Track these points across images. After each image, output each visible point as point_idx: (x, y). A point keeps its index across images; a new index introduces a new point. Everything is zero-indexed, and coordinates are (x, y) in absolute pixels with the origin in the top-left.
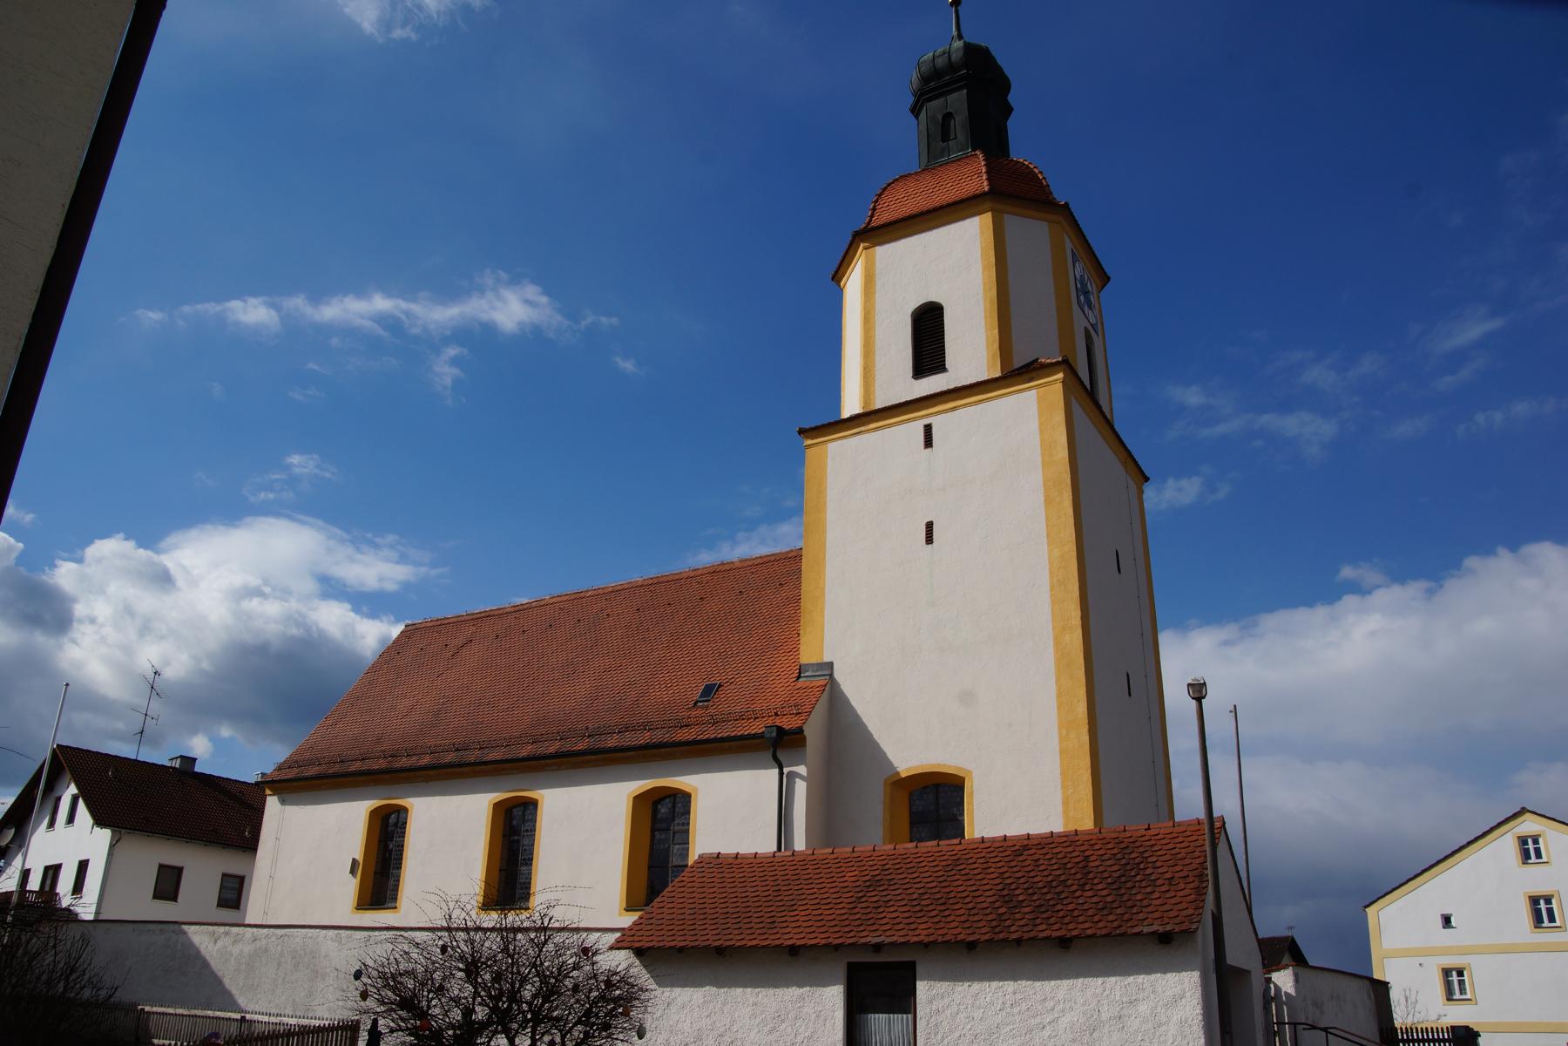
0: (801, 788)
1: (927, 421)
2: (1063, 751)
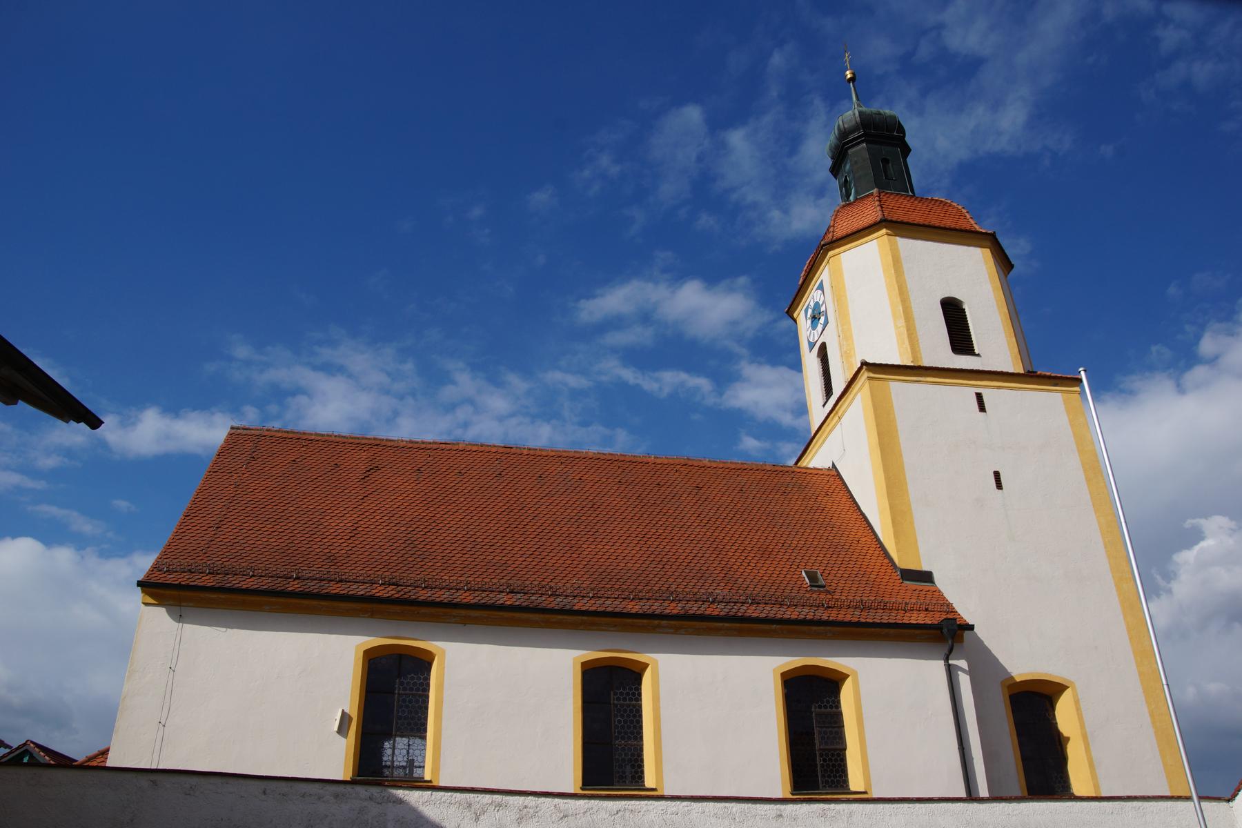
0: (964, 681)
1: (979, 390)
2: (1140, 674)
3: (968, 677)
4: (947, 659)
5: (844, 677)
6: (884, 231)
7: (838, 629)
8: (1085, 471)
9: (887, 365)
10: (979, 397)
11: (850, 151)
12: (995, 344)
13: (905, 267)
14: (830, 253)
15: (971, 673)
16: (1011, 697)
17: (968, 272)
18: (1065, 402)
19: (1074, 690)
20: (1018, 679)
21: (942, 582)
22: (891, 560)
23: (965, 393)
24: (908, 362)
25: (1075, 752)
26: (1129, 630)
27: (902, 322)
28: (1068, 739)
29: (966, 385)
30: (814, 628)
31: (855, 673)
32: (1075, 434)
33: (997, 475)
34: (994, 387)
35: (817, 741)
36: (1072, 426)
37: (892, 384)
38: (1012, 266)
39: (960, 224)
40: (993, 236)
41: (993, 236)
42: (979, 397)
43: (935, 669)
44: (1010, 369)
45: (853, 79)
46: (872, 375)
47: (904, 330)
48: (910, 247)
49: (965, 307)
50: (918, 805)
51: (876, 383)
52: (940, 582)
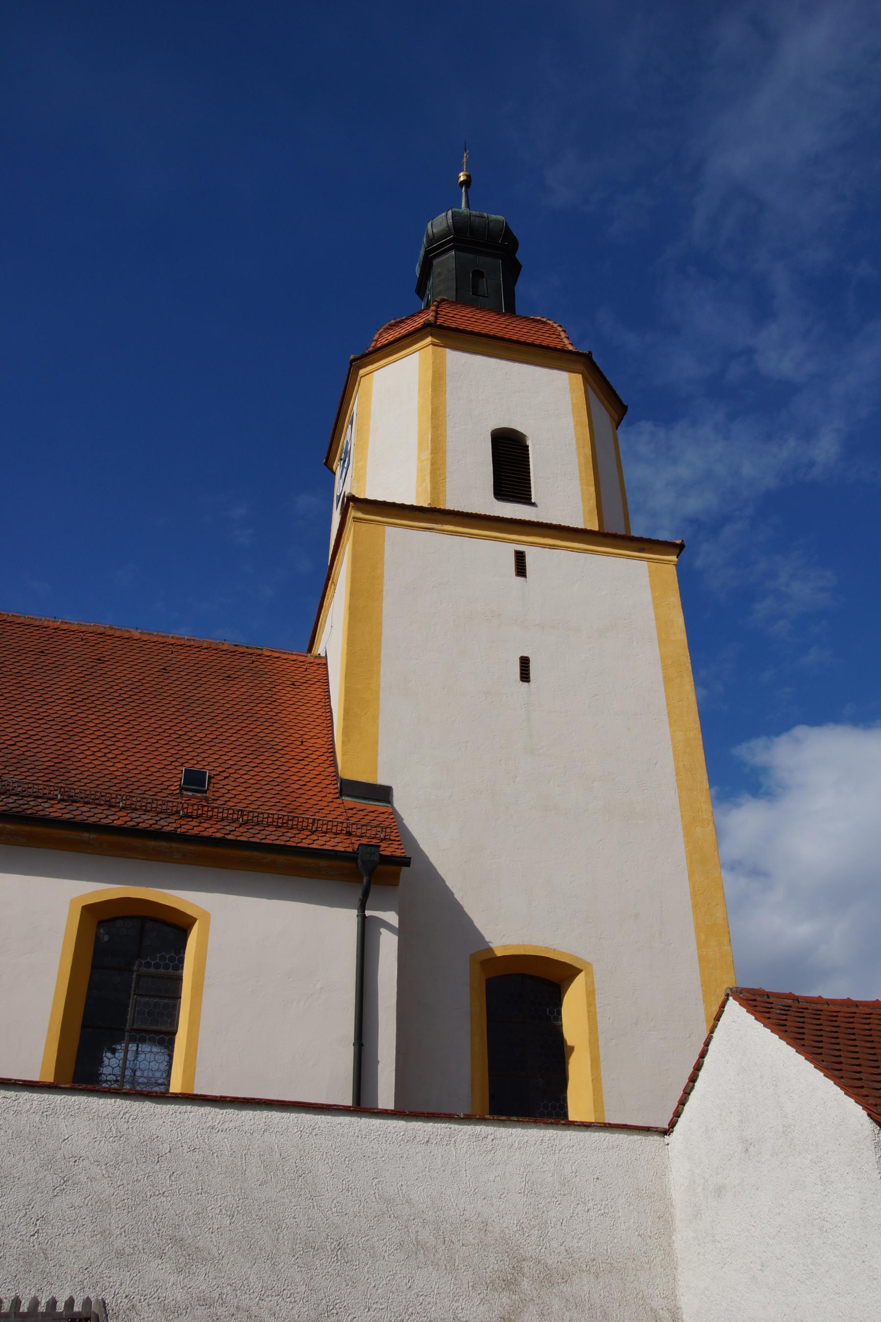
0: (388, 946)
1: (520, 548)
2: (702, 959)
3: (394, 939)
4: (362, 908)
5: (192, 921)
6: (429, 340)
7: (191, 848)
8: (665, 667)
9: (393, 505)
10: (520, 558)
11: (435, 262)
12: (562, 488)
13: (450, 385)
14: (362, 372)
15: (403, 932)
16: (489, 982)
17: (547, 404)
18: (649, 567)
19: (590, 975)
20: (499, 953)
21: (403, 803)
22: (334, 764)
23: (500, 551)
24: (424, 502)
25: (578, 1069)
26: (694, 893)
27: (427, 455)
28: (572, 1049)
29: (503, 540)
30: (152, 844)
31: (207, 915)
32: (657, 619)
33: (525, 663)
34: (544, 546)
35: (129, 1017)
36: (656, 606)
37: (389, 530)
38: (624, 409)
39: (552, 342)
40: (588, 357)
41: (588, 357)
42: (520, 558)
43: (343, 922)
44: (578, 523)
45: (467, 183)
46: (360, 515)
47: (428, 464)
48: (458, 361)
49: (529, 443)
50: (25, 1095)
51: (364, 526)
52: (400, 802)
